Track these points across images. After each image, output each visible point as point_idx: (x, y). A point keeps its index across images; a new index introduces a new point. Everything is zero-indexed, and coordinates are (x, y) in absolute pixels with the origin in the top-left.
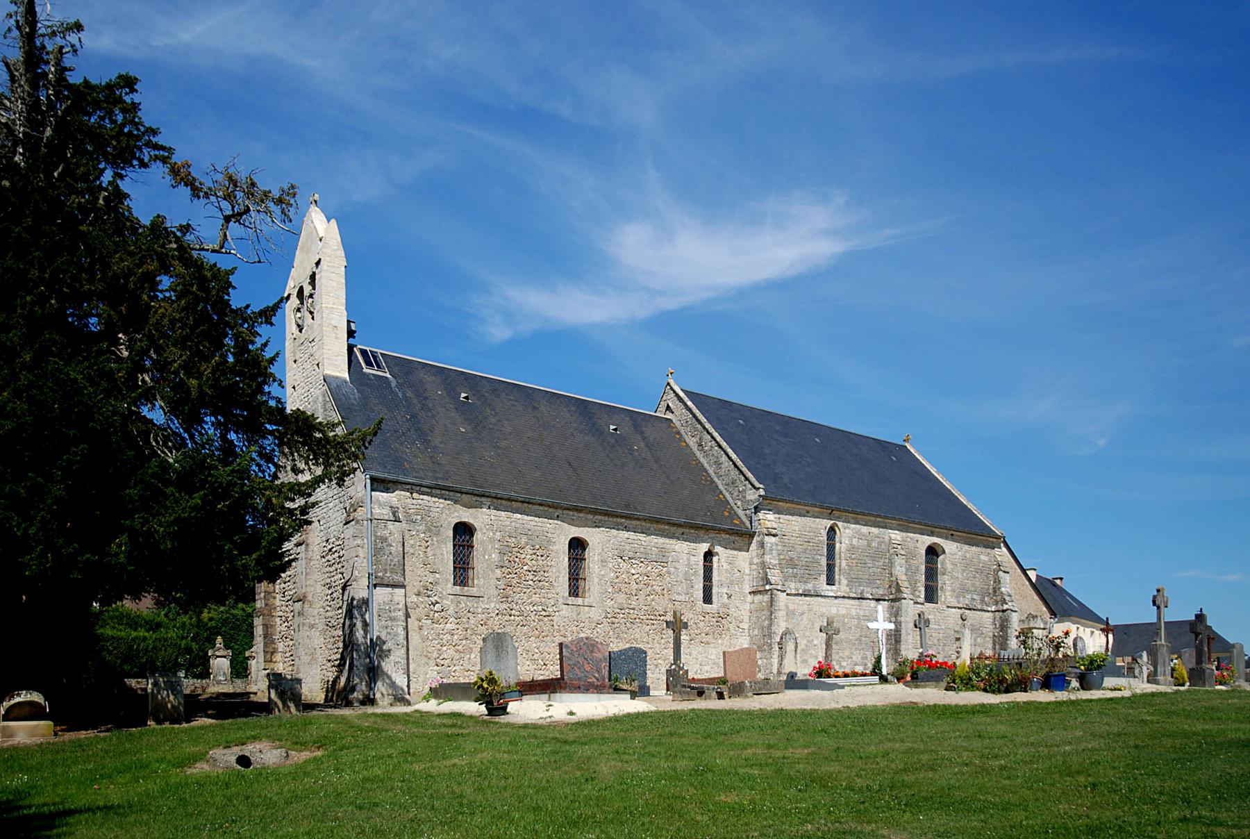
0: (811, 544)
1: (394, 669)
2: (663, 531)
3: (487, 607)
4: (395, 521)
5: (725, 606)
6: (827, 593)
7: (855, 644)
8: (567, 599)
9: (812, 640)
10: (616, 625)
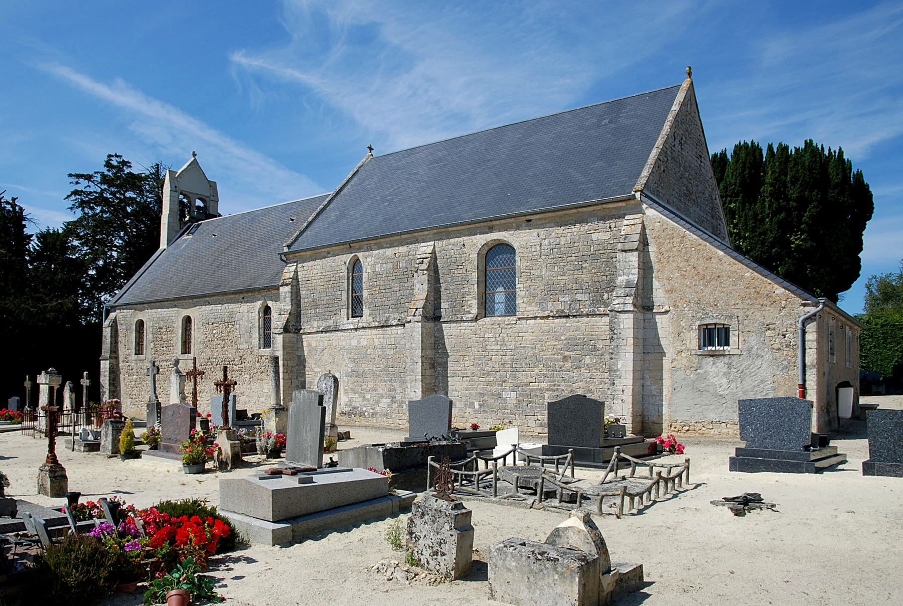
0: (332, 282)
2: (206, 301)
6: (346, 327)
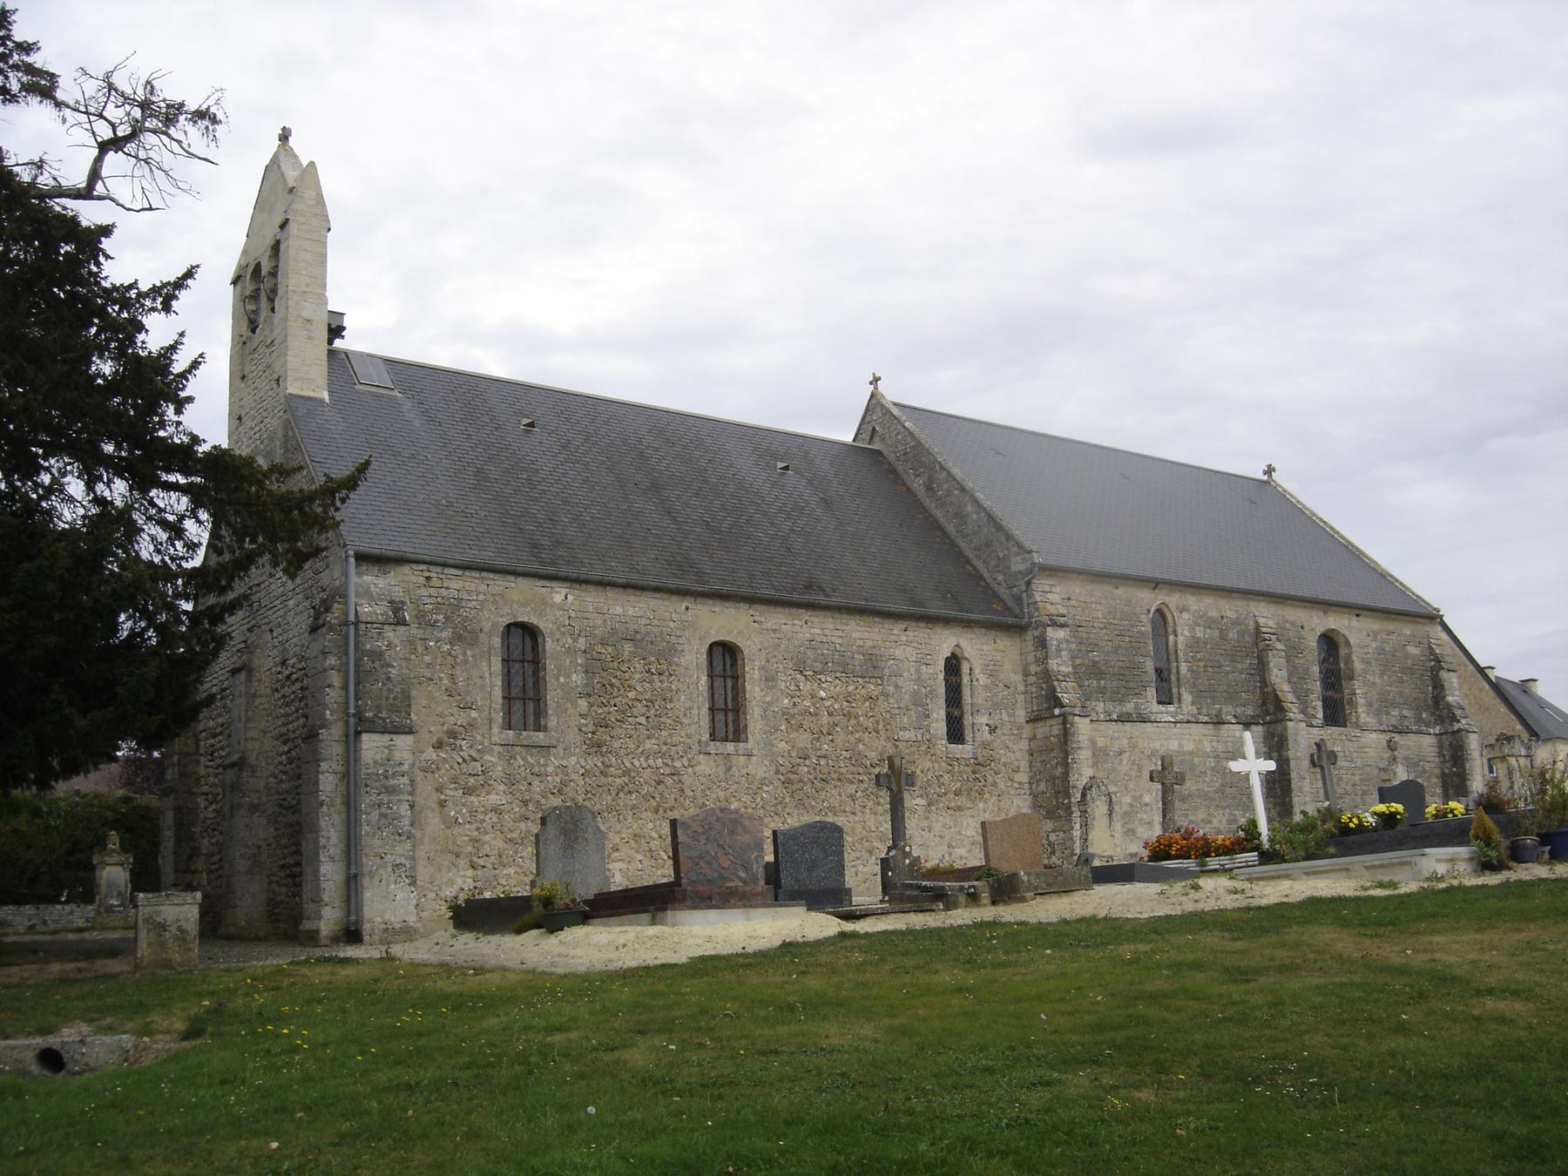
1: (393, 878)
3: (565, 764)
4: (398, 624)
5: (986, 745)
7: (1214, 799)
8: (707, 745)
9: (1141, 796)
10: (796, 786)
